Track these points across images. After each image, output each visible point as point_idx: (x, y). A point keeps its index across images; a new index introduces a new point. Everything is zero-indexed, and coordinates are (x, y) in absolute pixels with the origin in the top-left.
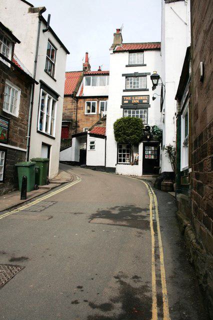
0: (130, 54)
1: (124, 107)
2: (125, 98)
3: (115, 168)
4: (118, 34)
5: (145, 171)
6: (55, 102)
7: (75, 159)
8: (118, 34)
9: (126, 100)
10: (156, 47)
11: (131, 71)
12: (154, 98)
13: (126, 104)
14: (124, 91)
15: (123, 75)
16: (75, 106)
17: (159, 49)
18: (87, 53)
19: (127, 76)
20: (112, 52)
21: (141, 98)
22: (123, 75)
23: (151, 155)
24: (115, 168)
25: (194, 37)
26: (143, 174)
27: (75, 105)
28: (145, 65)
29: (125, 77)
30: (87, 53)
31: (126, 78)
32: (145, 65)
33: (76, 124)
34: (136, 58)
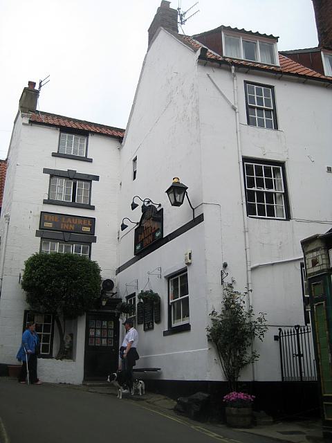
0: (62, 134)
1: (43, 233)
2: (46, 216)
4: (30, 94)
8: (30, 94)
10: (24, 124)
11: (64, 165)
14: (45, 202)
17: (120, 139)
18: (225, 266)
19: (54, 174)
20: (28, 122)
22: (46, 171)
23: (101, 338)
25: (116, 134)
26: (85, 379)
28: (90, 161)
30: (225, 266)
31: (52, 176)
32: (90, 161)
34: (73, 144)
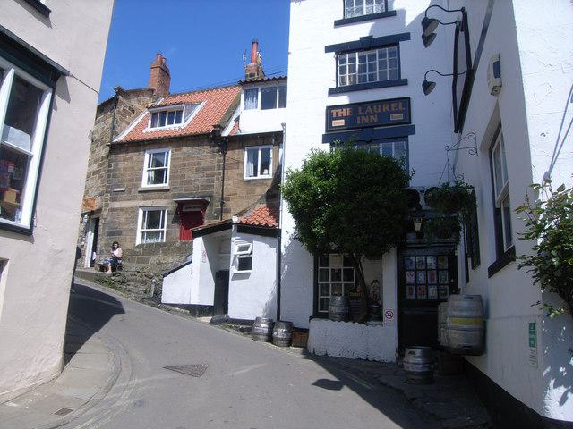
2: (334, 111)
3: (306, 331)
5: (405, 340)
6: (39, 95)
7: (199, 299)
9: (338, 118)
12: (427, 87)
13: (339, 128)
15: (328, 49)
16: (220, 161)
21: (386, 108)
22: (328, 49)
24: (306, 331)
27: (218, 157)
29: (333, 54)
33: (222, 204)
